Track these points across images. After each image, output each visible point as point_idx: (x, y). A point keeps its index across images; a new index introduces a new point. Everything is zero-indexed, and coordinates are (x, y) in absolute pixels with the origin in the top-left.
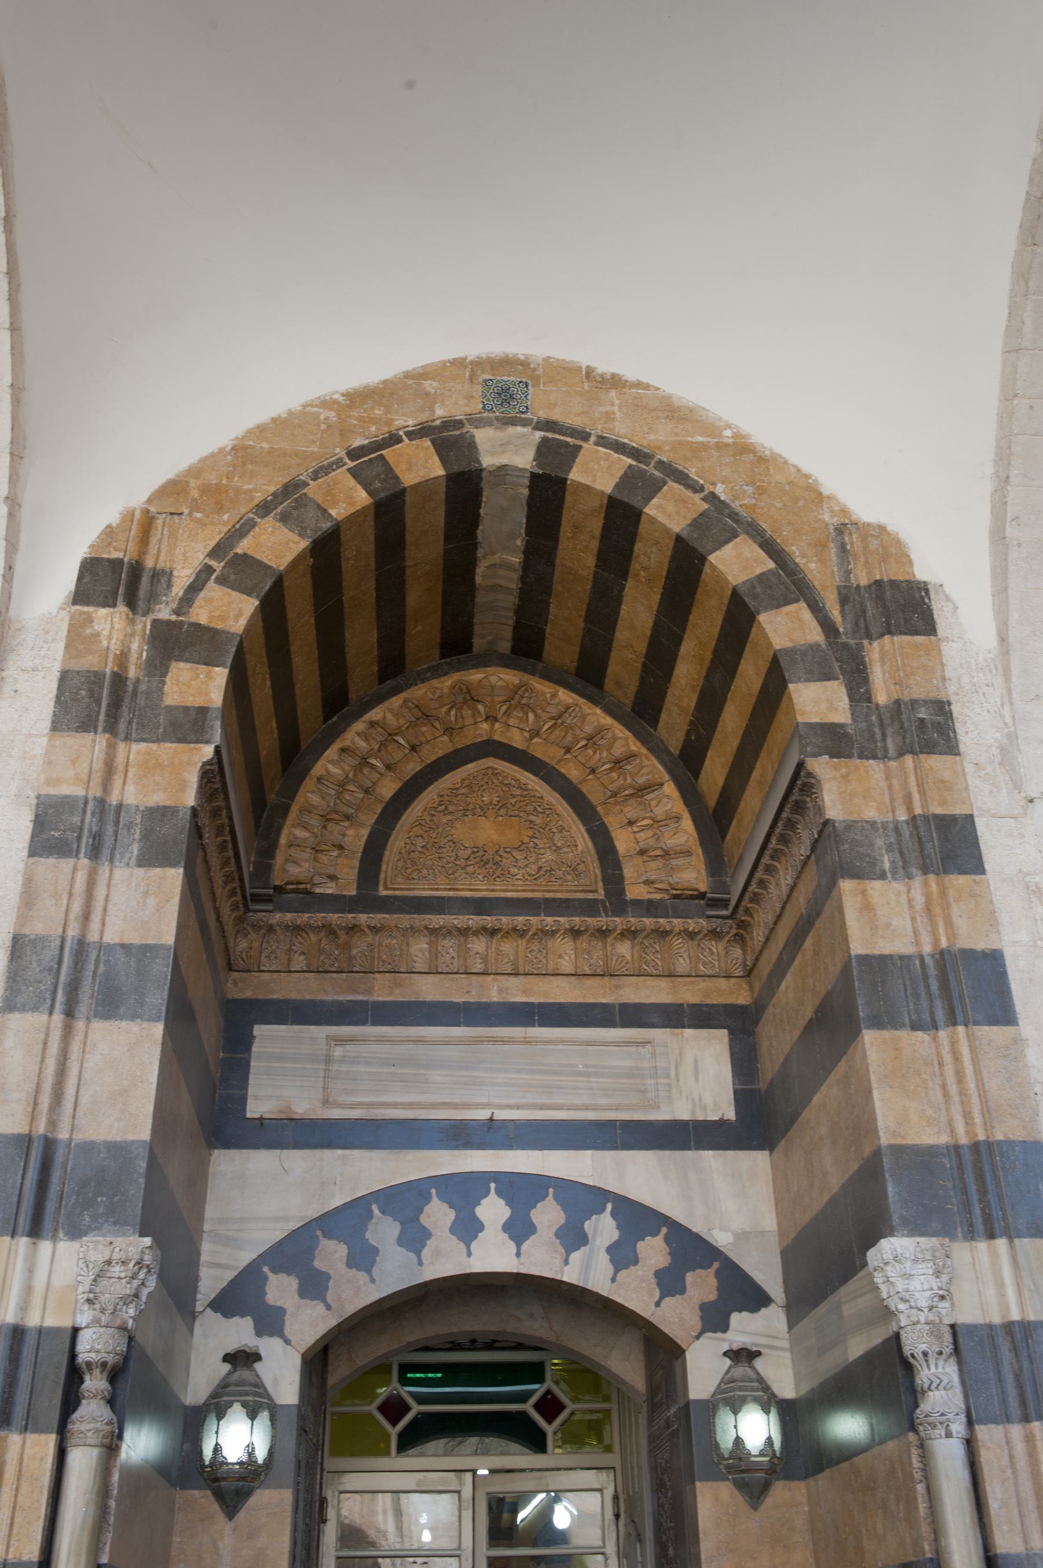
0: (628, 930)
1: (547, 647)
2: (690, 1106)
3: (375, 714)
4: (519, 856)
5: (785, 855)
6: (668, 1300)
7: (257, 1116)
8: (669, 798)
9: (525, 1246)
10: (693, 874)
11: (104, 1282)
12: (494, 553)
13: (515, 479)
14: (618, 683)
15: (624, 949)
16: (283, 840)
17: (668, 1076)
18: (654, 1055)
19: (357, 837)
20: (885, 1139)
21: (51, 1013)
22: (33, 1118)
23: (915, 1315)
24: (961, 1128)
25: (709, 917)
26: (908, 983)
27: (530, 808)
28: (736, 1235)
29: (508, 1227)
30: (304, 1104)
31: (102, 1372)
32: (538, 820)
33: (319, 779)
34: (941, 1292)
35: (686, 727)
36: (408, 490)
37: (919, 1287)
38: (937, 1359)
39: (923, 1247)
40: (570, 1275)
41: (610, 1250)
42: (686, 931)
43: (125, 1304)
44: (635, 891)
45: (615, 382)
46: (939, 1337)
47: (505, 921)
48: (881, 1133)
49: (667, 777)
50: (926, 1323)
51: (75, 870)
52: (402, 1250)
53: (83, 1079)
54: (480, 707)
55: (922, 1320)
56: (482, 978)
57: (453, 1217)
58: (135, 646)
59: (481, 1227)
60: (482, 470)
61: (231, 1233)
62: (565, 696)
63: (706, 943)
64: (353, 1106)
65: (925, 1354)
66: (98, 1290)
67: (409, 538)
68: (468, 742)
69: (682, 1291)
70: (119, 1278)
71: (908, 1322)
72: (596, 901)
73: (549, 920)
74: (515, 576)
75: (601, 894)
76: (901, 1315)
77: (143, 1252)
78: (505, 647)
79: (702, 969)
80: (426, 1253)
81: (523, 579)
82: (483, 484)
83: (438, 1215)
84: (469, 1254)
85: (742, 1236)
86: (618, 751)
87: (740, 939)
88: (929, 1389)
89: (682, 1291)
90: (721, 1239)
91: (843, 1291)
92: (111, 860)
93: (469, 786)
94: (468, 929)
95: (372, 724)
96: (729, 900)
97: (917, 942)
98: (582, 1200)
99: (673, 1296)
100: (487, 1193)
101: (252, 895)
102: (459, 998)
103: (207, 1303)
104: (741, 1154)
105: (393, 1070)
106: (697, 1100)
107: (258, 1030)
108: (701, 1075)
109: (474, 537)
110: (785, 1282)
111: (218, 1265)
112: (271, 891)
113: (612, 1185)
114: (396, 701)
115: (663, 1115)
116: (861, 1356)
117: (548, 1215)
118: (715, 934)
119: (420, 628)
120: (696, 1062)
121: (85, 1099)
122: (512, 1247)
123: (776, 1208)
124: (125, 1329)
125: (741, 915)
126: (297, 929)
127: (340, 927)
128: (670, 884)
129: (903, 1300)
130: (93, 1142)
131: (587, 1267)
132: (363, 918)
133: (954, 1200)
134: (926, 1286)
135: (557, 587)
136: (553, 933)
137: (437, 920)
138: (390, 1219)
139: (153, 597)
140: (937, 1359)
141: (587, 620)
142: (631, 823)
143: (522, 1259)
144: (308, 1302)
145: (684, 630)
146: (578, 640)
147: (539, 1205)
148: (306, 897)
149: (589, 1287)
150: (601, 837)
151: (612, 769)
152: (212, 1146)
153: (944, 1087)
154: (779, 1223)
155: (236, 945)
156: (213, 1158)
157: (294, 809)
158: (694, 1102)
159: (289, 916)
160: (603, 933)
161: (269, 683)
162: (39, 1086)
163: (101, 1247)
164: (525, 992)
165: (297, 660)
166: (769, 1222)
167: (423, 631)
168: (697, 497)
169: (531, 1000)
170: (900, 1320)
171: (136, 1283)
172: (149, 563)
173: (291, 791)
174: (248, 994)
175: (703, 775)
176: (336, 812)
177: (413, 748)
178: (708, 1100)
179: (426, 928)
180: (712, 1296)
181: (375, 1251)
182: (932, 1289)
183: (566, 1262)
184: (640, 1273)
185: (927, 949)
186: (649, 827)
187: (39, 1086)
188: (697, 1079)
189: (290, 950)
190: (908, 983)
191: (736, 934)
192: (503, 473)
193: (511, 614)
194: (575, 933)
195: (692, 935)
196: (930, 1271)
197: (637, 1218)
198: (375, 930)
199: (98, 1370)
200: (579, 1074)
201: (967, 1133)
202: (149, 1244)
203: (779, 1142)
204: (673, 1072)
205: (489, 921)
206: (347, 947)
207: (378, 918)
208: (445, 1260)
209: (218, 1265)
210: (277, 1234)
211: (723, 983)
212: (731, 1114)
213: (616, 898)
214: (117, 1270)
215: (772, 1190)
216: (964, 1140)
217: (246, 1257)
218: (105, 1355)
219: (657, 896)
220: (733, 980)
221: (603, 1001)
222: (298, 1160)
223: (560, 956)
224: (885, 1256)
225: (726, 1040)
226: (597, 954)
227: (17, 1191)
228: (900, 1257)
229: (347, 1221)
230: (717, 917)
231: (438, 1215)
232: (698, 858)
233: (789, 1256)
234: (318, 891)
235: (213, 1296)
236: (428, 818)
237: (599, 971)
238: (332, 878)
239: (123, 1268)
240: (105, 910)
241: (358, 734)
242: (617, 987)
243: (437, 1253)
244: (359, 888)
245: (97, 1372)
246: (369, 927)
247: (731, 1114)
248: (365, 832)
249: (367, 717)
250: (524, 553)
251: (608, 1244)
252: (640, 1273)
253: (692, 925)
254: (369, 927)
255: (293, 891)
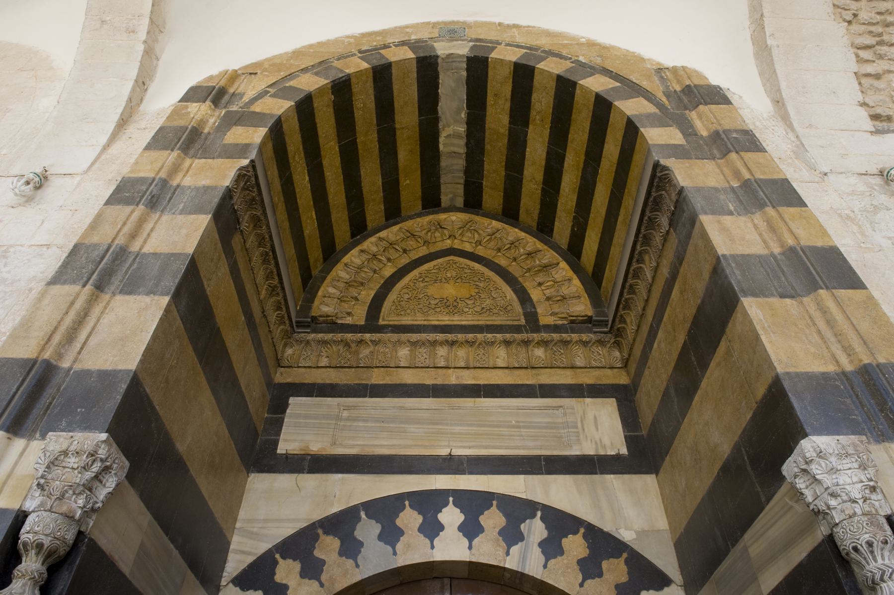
0: (543, 341)
1: (485, 197)
2: (594, 446)
3: (383, 234)
4: (469, 302)
5: (648, 252)
6: (589, 581)
7: (284, 452)
8: (564, 269)
9: (476, 541)
10: (582, 307)
11: (57, 471)
12: (449, 126)
13: (458, 64)
14: (527, 211)
15: (540, 352)
16: (320, 293)
17: (576, 427)
18: (565, 414)
19: (368, 295)
20: (780, 369)
21: (84, 286)
22: (43, 349)
23: (849, 508)
24: (844, 360)
25: (595, 332)
26: (768, 270)
27: (476, 279)
28: (637, 533)
29: (462, 528)
30: (318, 445)
31: (37, 554)
32: (481, 285)
33: (346, 265)
34: (872, 483)
35: (571, 224)
36: (393, 65)
37: (849, 481)
38: (882, 549)
39: (844, 443)
40: (511, 563)
41: (541, 544)
42: (581, 341)
43: (74, 494)
44: (544, 320)
45: (515, 26)
46: (881, 528)
47: (461, 337)
48: (775, 364)
49: (561, 259)
50: (863, 514)
51: (132, 212)
52: (382, 544)
53: (96, 329)
54: (446, 232)
55: (858, 511)
56: (445, 371)
57: (421, 521)
58: (212, 121)
59: (441, 527)
60: (437, 57)
61: (255, 530)
62: (495, 224)
63: (594, 349)
64: (352, 446)
65: (870, 544)
66: (50, 476)
67: (396, 105)
68: (438, 249)
69: (600, 575)
70: (72, 468)
71: (843, 517)
72: (520, 326)
73: (489, 335)
74: (462, 142)
75: (523, 321)
76: (833, 512)
77: (97, 445)
78: (460, 202)
79: (596, 361)
80: (399, 546)
81: (467, 145)
82: (439, 68)
83: (410, 519)
84: (433, 547)
85: (642, 534)
86: (529, 248)
87: (618, 344)
88: (882, 580)
89: (600, 575)
90: (627, 536)
91: (746, 536)
92: (162, 211)
93: (439, 269)
94: (435, 341)
95: (380, 239)
96: (608, 321)
97: (767, 246)
98: (518, 510)
99: (593, 578)
100: (446, 504)
101: (297, 322)
102: (429, 382)
103: (229, 579)
104: (635, 477)
105: (382, 424)
106: (598, 442)
107: (292, 400)
108: (601, 428)
109: (436, 112)
110: (680, 567)
111: (243, 552)
112: (309, 320)
113: (540, 498)
114: (395, 228)
115: (575, 451)
116: (781, 583)
117: (492, 520)
118: (601, 342)
119: (408, 182)
120: (595, 418)
121: (93, 341)
122: (466, 542)
123: (666, 513)
124: (72, 518)
125: (618, 325)
126: (325, 343)
127: (352, 341)
128: (568, 313)
129: (834, 495)
130: (89, 370)
131: (523, 558)
132: (367, 336)
133: (856, 412)
134: (855, 479)
135: (488, 147)
136: (493, 343)
137: (415, 337)
138: (374, 521)
139: (229, 103)
140: (882, 549)
141: (506, 169)
142: (540, 284)
143: (473, 551)
144: (307, 581)
145: (565, 151)
146: (502, 187)
147: (486, 512)
148: (333, 326)
149: (526, 572)
150: (524, 297)
151: (526, 259)
152: (249, 471)
153: (819, 332)
154: (670, 524)
155: (283, 352)
156: (249, 479)
157: (329, 278)
158: (596, 443)
159: (320, 336)
160: (526, 343)
161: (307, 178)
162: (56, 328)
163: (62, 439)
164: (474, 378)
165: (328, 174)
166: (662, 523)
167: (411, 185)
168: (568, 62)
169: (478, 383)
170: (832, 517)
171: (89, 475)
172: (231, 90)
173: (327, 271)
174: (289, 380)
175: (582, 258)
176: (355, 281)
177: (405, 251)
178: (606, 441)
179: (409, 341)
180: (624, 578)
181: (361, 544)
182: (862, 482)
183: (508, 554)
184: (565, 561)
185: (777, 250)
186: (553, 286)
187: (56, 328)
188: (597, 429)
189: (319, 355)
190: (768, 270)
191: (615, 342)
192: (450, 60)
193: (462, 175)
194: (507, 343)
195: (585, 344)
196: (856, 465)
197: (561, 523)
198: (375, 343)
199: (33, 552)
200: (513, 427)
201: (851, 362)
202: (104, 438)
203: (663, 460)
204: (579, 425)
205: (450, 337)
206: (357, 353)
207: (376, 336)
208: (414, 551)
209: (243, 552)
210: (288, 530)
211: (609, 372)
212: (624, 451)
213: (532, 322)
214: (72, 461)
215: (661, 501)
216: (849, 368)
217: (263, 547)
218: (43, 537)
219: (560, 322)
220: (615, 370)
221: (528, 383)
222: (310, 481)
223: (497, 357)
224: (808, 455)
225: (615, 404)
226: (521, 356)
227: (9, 398)
228: (824, 452)
229: (341, 524)
230: (601, 332)
231: (410, 519)
232: (585, 298)
233: (682, 546)
234: (339, 322)
235: (235, 574)
236: (412, 285)
237: (524, 365)
238: (349, 314)
239: (77, 460)
240: (149, 235)
241: (372, 243)
242: (537, 375)
243: (408, 546)
244: (366, 320)
245: (33, 553)
246: (371, 341)
247: (624, 451)
248: (372, 293)
249: (377, 235)
250: (467, 124)
251: (539, 540)
252: (565, 561)
253: (584, 337)
254: (371, 341)
255: (324, 322)
